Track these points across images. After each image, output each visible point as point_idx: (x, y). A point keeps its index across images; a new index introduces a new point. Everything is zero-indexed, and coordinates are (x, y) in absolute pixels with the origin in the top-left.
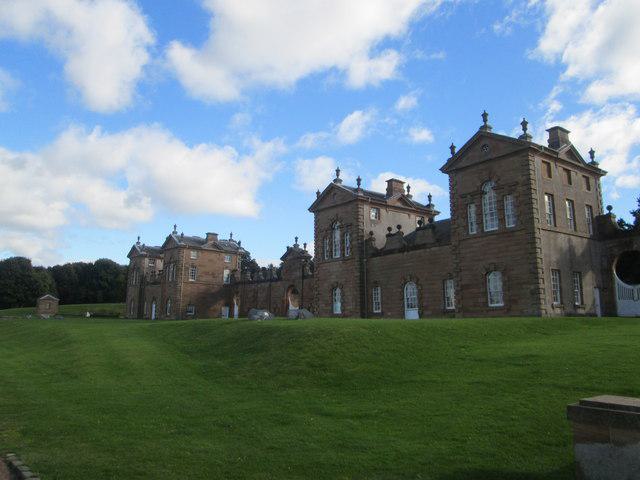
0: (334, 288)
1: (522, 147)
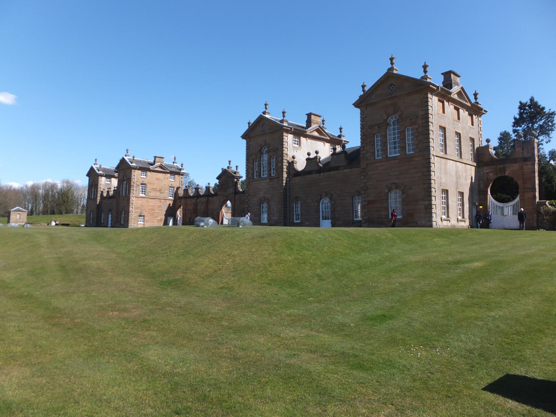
0: (261, 202)
1: (422, 87)
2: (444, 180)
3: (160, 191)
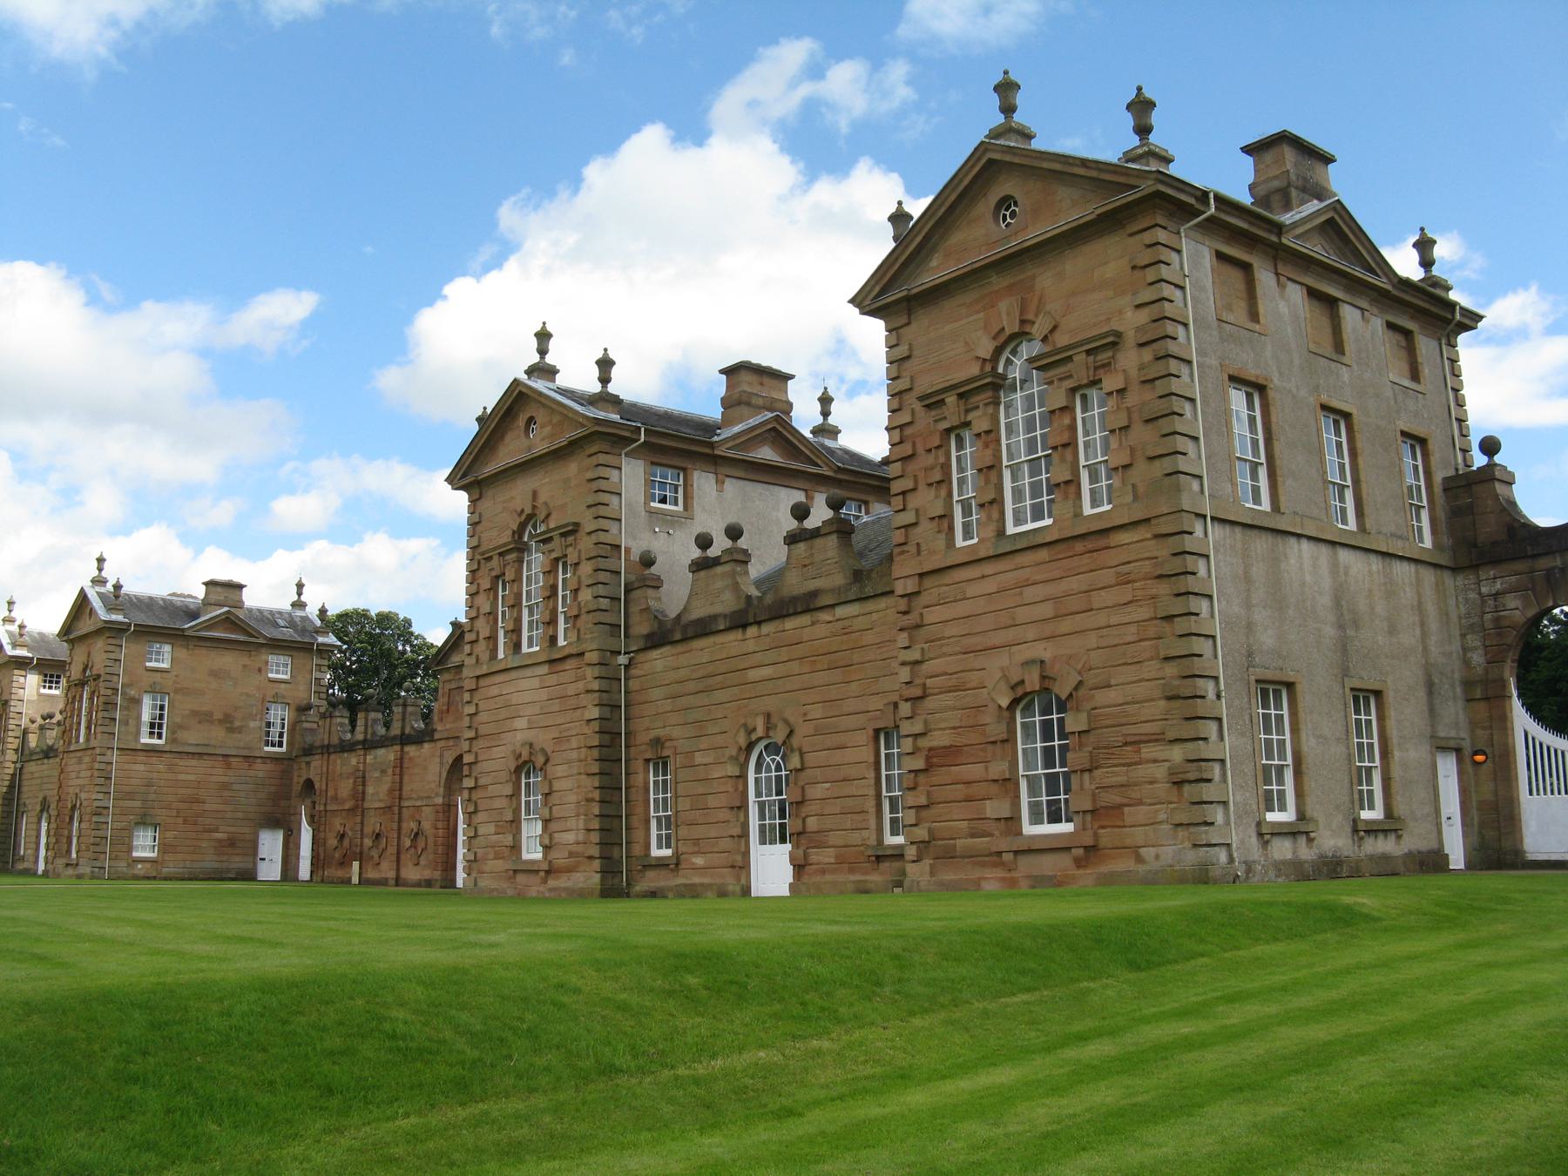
2: (1267, 639)
3: (227, 721)
